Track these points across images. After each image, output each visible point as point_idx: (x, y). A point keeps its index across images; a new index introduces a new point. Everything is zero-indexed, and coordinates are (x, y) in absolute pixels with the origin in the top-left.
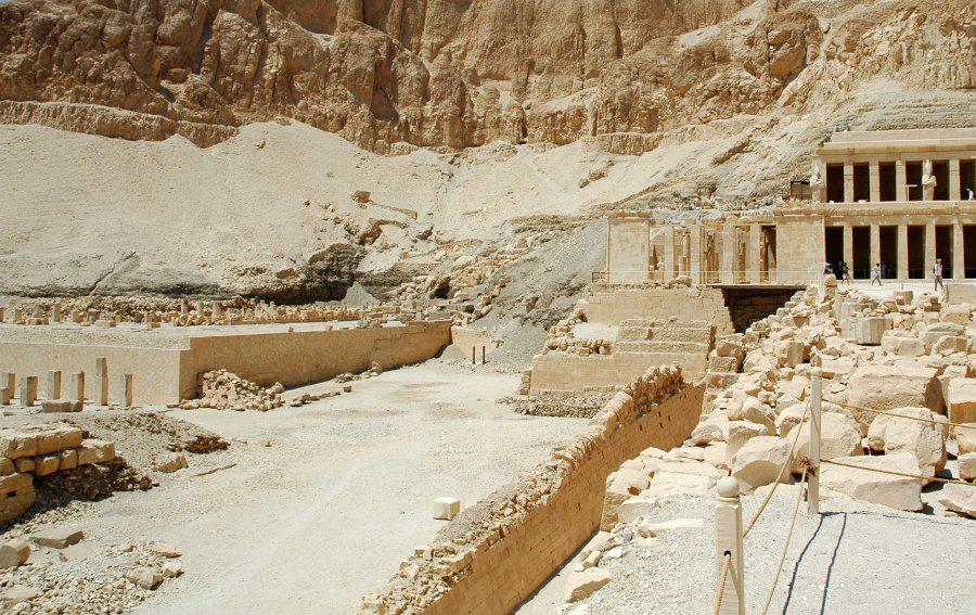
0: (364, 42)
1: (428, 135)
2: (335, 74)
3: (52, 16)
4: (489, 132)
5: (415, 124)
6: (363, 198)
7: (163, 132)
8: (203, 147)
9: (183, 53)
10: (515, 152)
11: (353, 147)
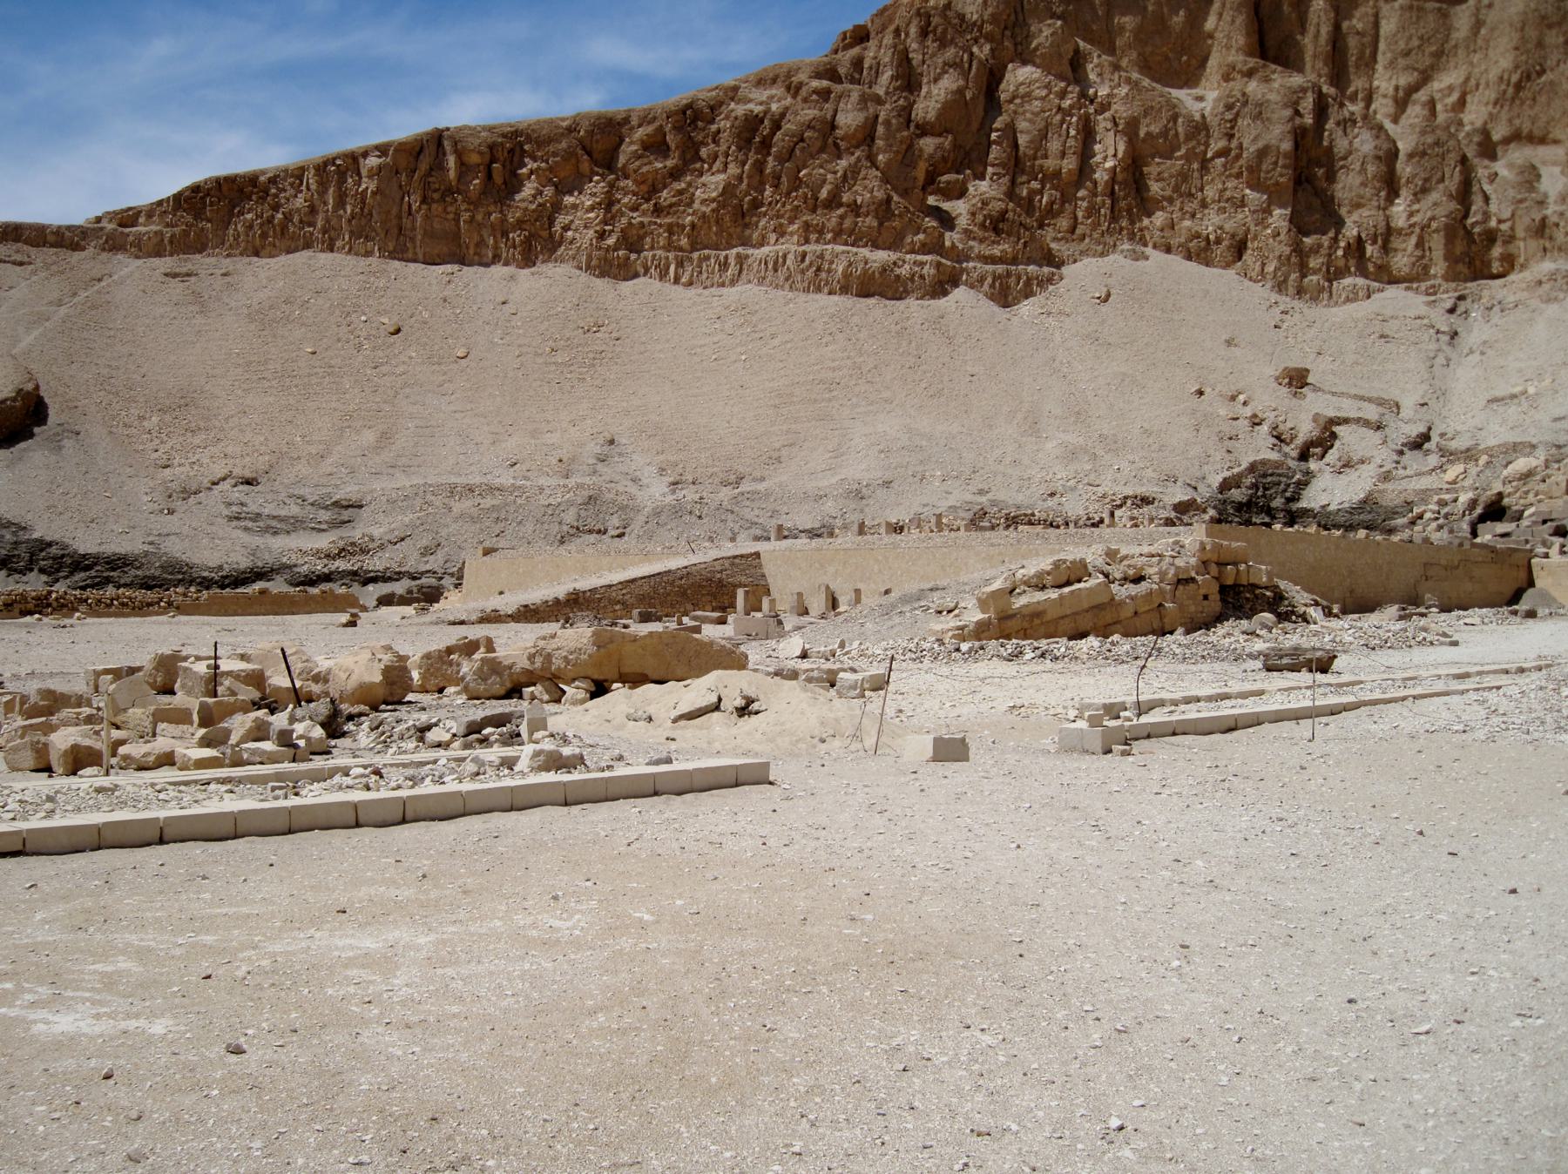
0: (1273, 97)
1: (1401, 261)
2: (1219, 161)
3: (758, 109)
4: (1522, 247)
5: (1374, 242)
6: (1297, 380)
7: (941, 283)
8: (1006, 306)
9: (956, 146)
11: (1261, 293)
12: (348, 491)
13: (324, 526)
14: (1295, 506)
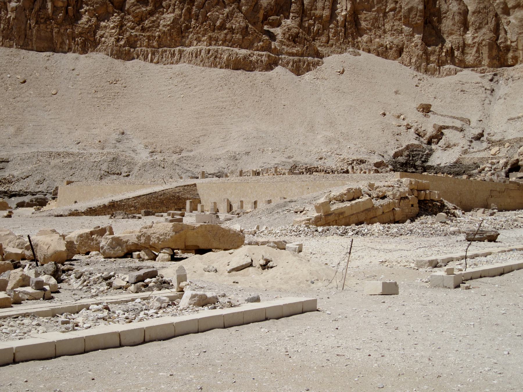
1: (470, 58)
2: (392, 13)
5: (458, 50)
6: (426, 109)
10: (172, 285)
11: (410, 71)
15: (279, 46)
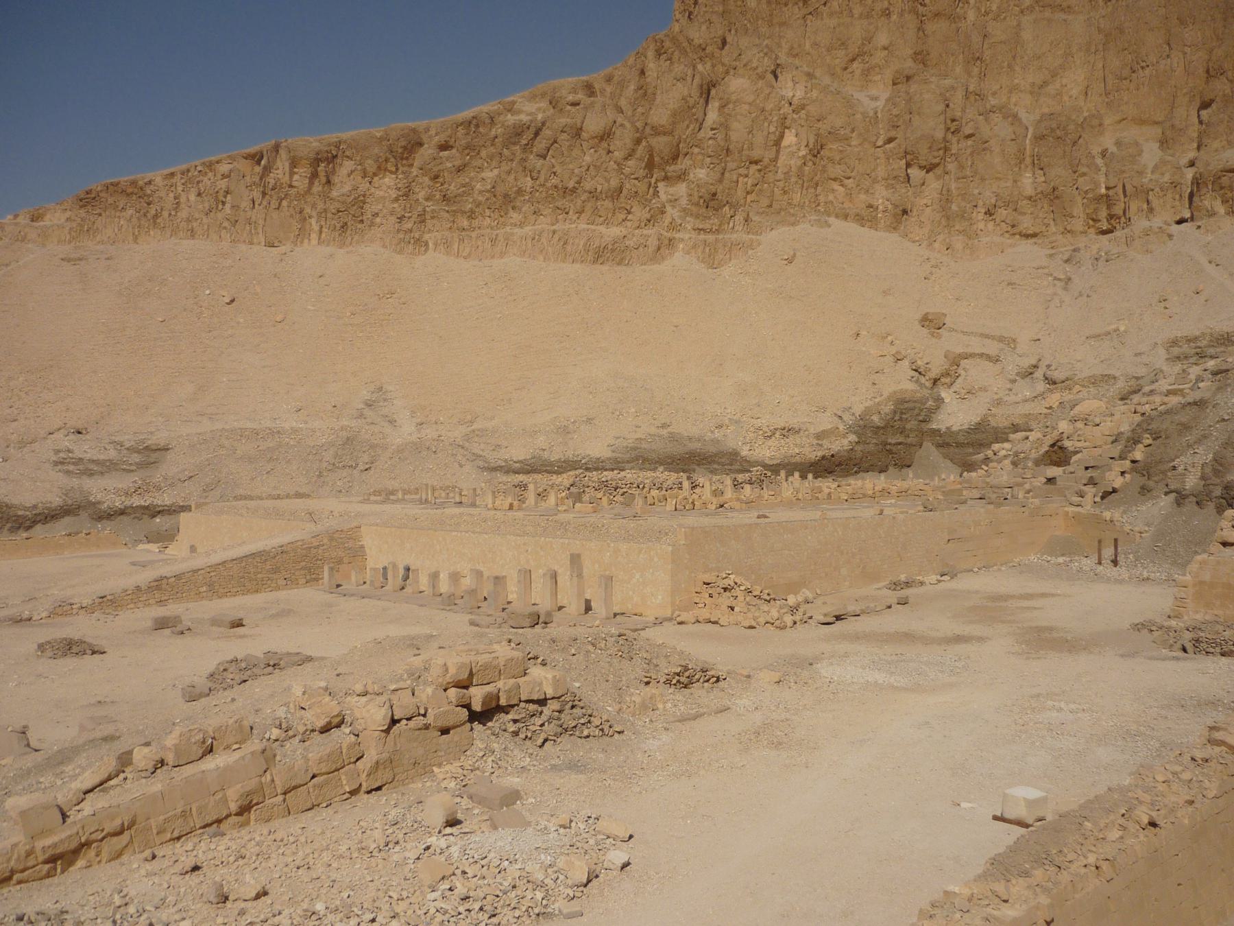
3: (524, 118)
12: (160, 438)
13: (133, 468)
14: (926, 427)
15: (680, 217)
